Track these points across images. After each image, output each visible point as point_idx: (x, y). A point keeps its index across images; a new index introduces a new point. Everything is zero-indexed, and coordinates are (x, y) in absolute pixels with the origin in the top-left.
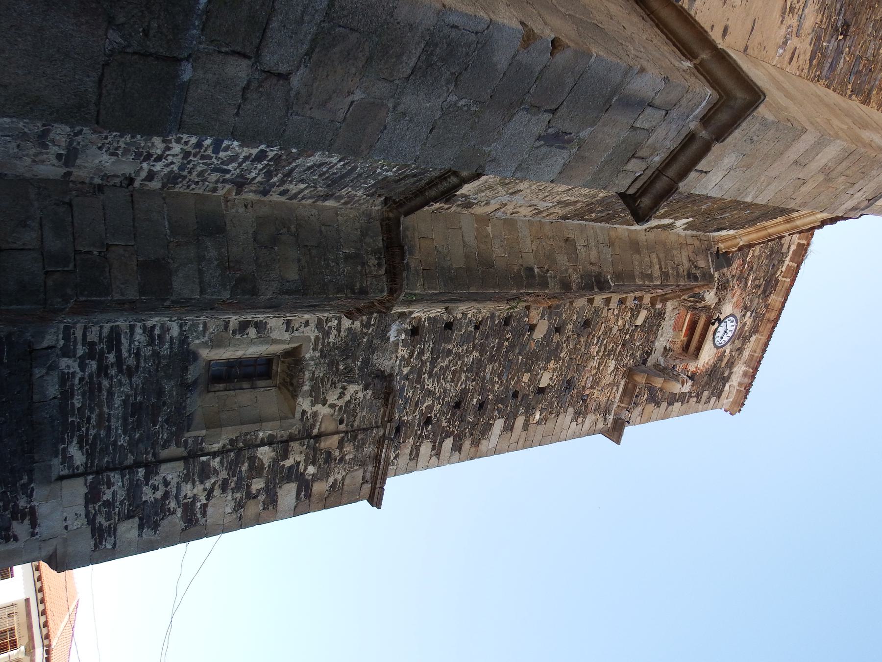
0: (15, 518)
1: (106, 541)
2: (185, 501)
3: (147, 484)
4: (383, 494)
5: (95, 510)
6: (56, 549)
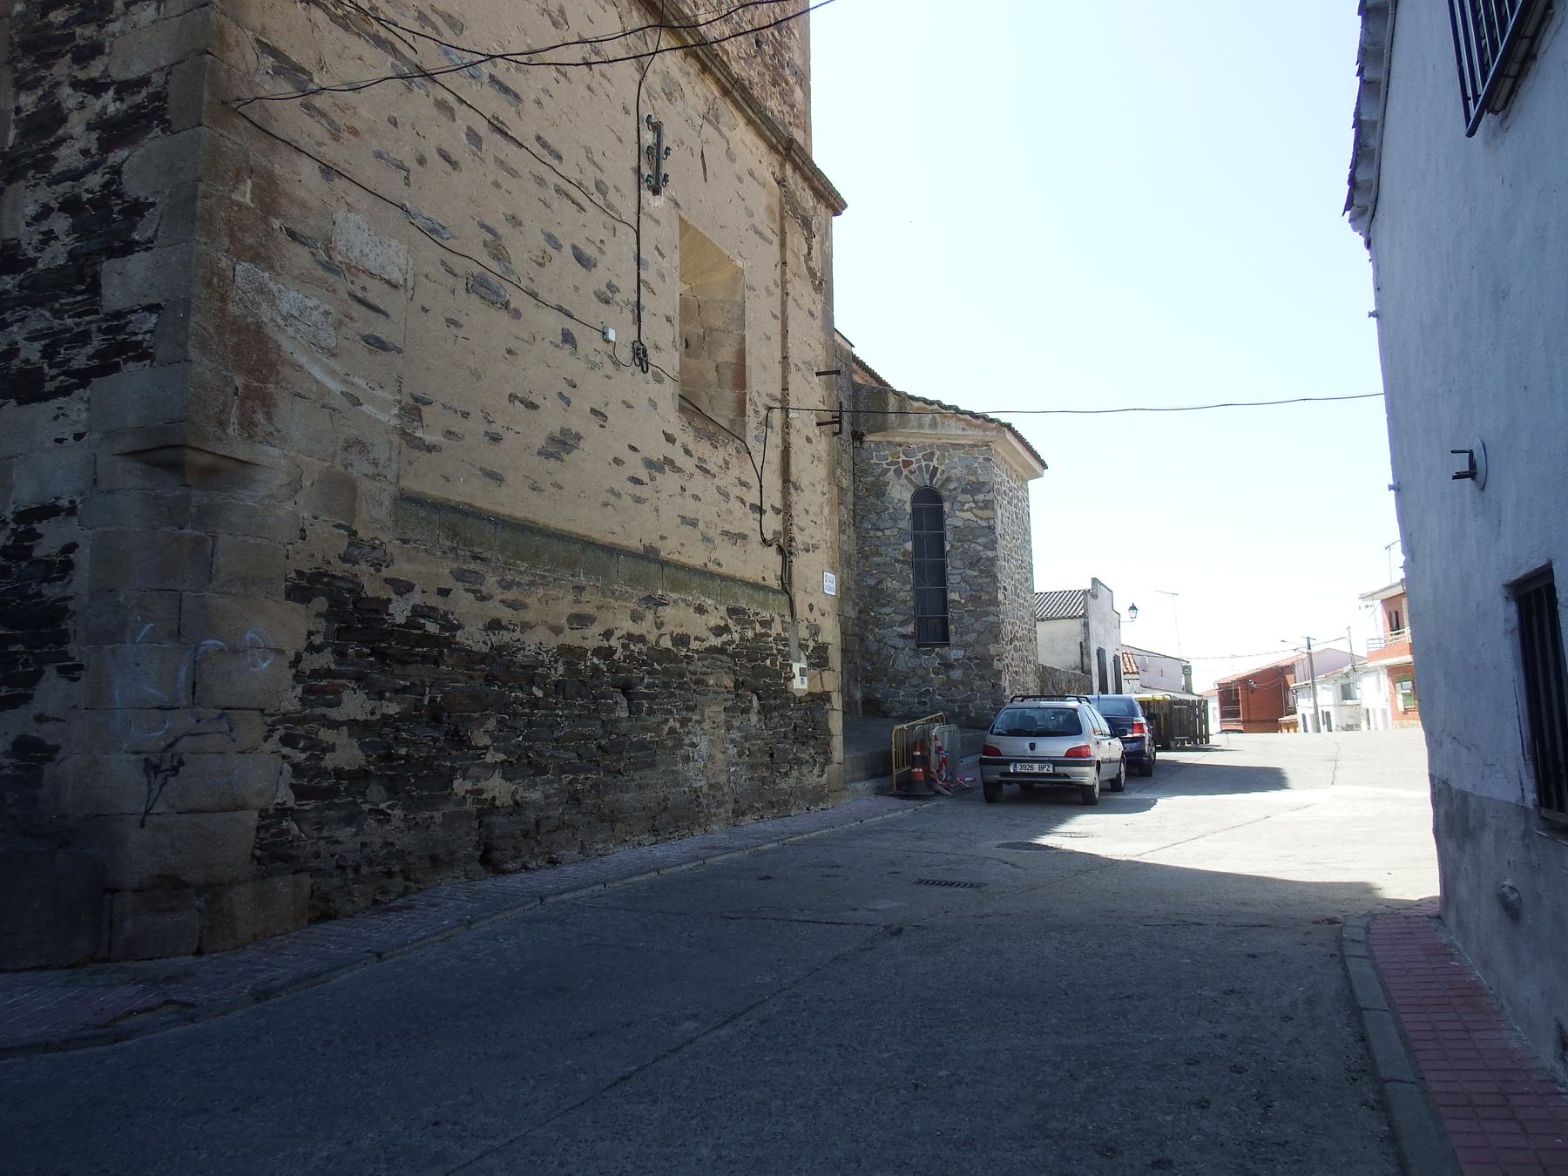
0: (26, 554)
1: (136, 334)
2: (93, 151)
3: (33, 262)
4: (1392, 448)
5: (59, 375)
6: (125, 454)
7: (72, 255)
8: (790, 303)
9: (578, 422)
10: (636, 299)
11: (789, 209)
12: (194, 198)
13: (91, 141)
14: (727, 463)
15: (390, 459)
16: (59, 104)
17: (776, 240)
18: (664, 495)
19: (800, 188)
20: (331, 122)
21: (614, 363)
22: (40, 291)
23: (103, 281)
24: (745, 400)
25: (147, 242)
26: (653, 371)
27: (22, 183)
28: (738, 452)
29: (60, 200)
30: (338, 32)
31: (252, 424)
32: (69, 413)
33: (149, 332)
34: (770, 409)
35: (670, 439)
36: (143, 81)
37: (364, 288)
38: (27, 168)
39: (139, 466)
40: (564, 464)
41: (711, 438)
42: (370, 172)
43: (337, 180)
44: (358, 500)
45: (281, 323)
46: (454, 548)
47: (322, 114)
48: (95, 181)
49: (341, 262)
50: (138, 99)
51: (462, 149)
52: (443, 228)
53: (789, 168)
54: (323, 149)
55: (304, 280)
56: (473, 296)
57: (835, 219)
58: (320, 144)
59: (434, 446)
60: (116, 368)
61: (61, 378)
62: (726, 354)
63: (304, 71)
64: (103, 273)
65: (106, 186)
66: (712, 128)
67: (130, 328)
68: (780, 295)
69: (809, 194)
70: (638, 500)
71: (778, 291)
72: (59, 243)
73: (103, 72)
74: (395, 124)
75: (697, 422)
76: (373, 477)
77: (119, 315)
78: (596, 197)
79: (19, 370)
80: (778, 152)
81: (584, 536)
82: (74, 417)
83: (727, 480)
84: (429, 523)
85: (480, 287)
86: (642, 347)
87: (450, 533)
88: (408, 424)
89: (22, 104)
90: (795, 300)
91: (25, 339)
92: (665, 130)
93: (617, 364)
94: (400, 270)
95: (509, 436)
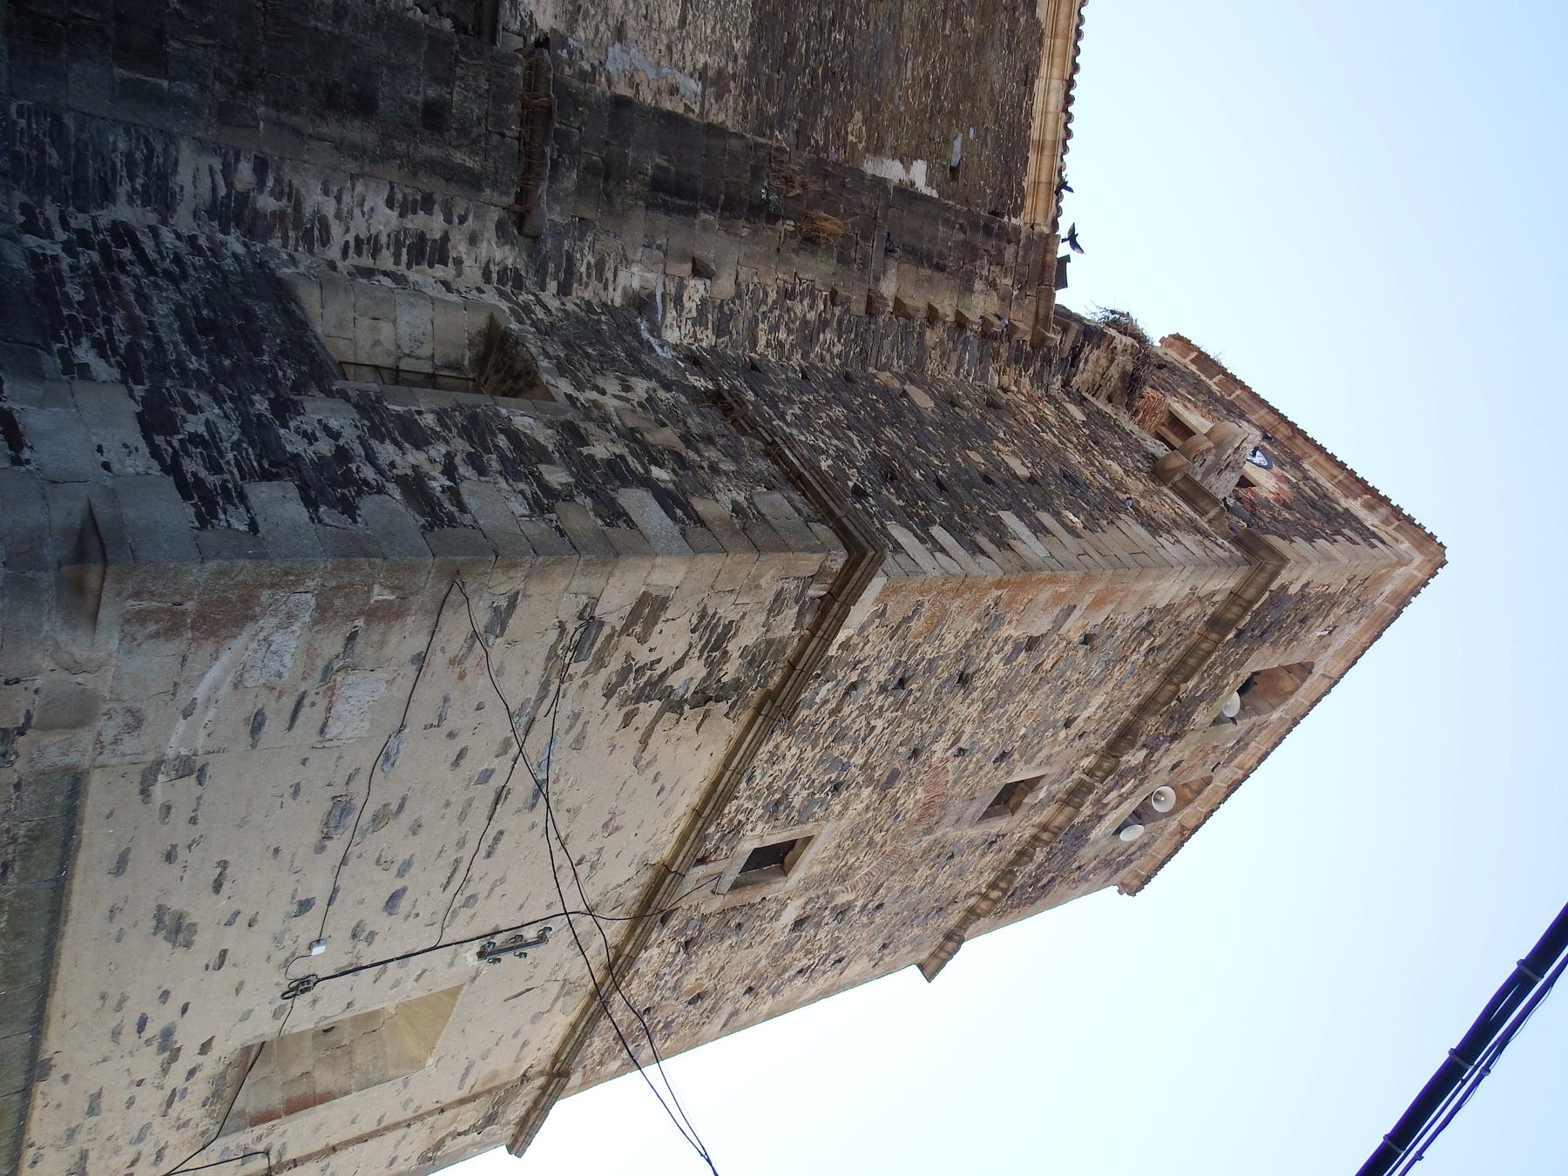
1: (225, 513)
7: (296, 457)
8: (400, 1133)
9: (206, 943)
10: (364, 965)
11: (500, 1095)
12: (367, 555)
13: (403, 469)
14: (185, 1125)
15: (123, 755)
16: (431, 444)
17: (464, 1093)
18: (128, 1062)
19: (525, 1099)
20: (465, 657)
21: (287, 960)
22: (256, 432)
23: (275, 483)
24: (272, 1120)
25: (318, 518)
26: (286, 1005)
27: (357, 416)
28: (203, 1134)
29: (346, 446)
30: (544, 653)
31: (143, 622)
32: (132, 456)
33: (229, 525)
34: (267, 1153)
35: (205, 1048)
36: (463, 508)
37: (313, 704)
38: (371, 420)
39: (78, 522)
40: (151, 936)
41: (216, 1094)
42: (428, 695)
43: (414, 667)
44: (68, 731)
45: (261, 636)
46: (16, 840)
47: (470, 649)
48: (369, 473)
49: (335, 681)
50: (447, 504)
51: (471, 767)
52: (393, 765)
53: (541, 1081)
54: (439, 654)
55: (310, 652)
56: (331, 804)
57: (502, 1150)
58: (443, 650)
59: (149, 796)
60: (186, 496)
61: (170, 450)
62: (325, 1080)
63: (503, 630)
64: (283, 482)
65: (366, 482)
66: (557, 991)
67: (229, 507)
68: (406, 1118)
69: (521, 1111)
70: (116, 1034)
71: (410, 1114)
72: (306, 446)
73: (464, 476)
74: (478, 709)
75: (232, 1074)
76: (98, 741)
77: (243, 498)
78: (460, 899)
79: (173, 415)
80: (554, 1065)
81: (55, 983)
82: (128, 462)
83: (163, 1132)
84: (47, 808)
85: (341, 808)
86: (312, 985)
87: (37, 833)
88: (172, 767)
89: (425, 416)
90: (404, 1137)
91: (207, 420)
92: (543, 947)
93: (287, 963)
94: (341, 733)
95: (175, 869)
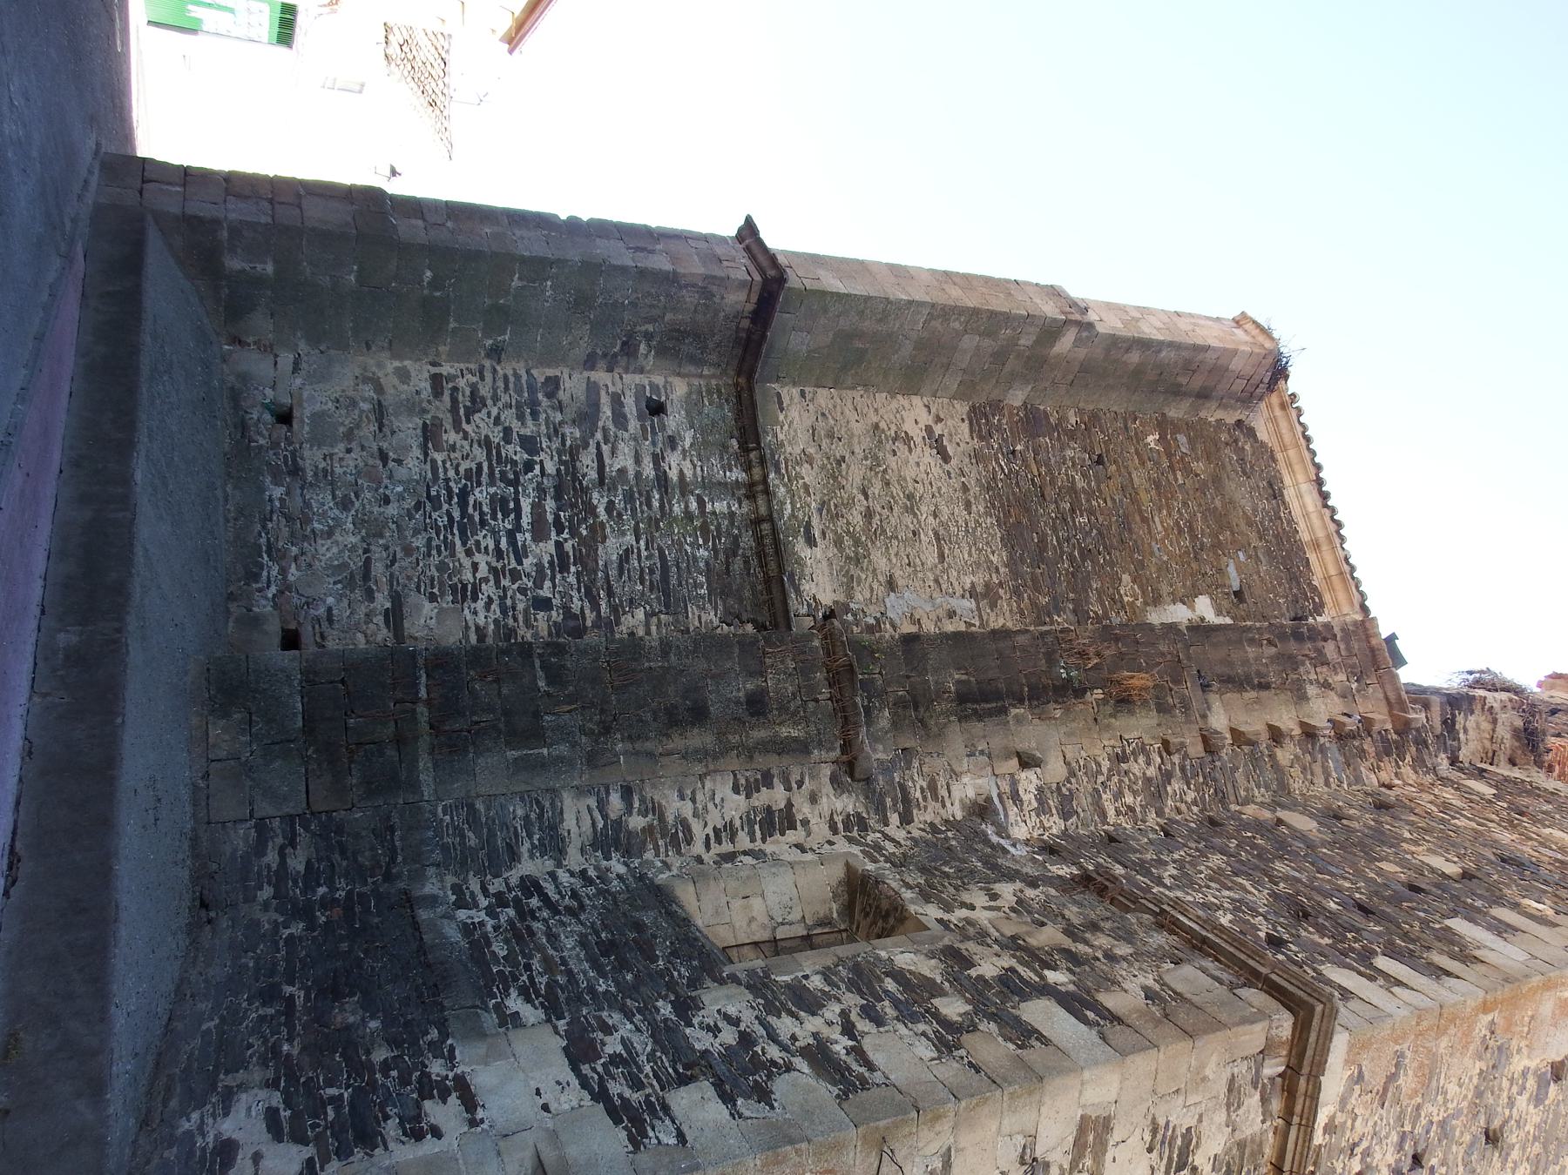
1: (653, 1130)
5: (598, 1073)
